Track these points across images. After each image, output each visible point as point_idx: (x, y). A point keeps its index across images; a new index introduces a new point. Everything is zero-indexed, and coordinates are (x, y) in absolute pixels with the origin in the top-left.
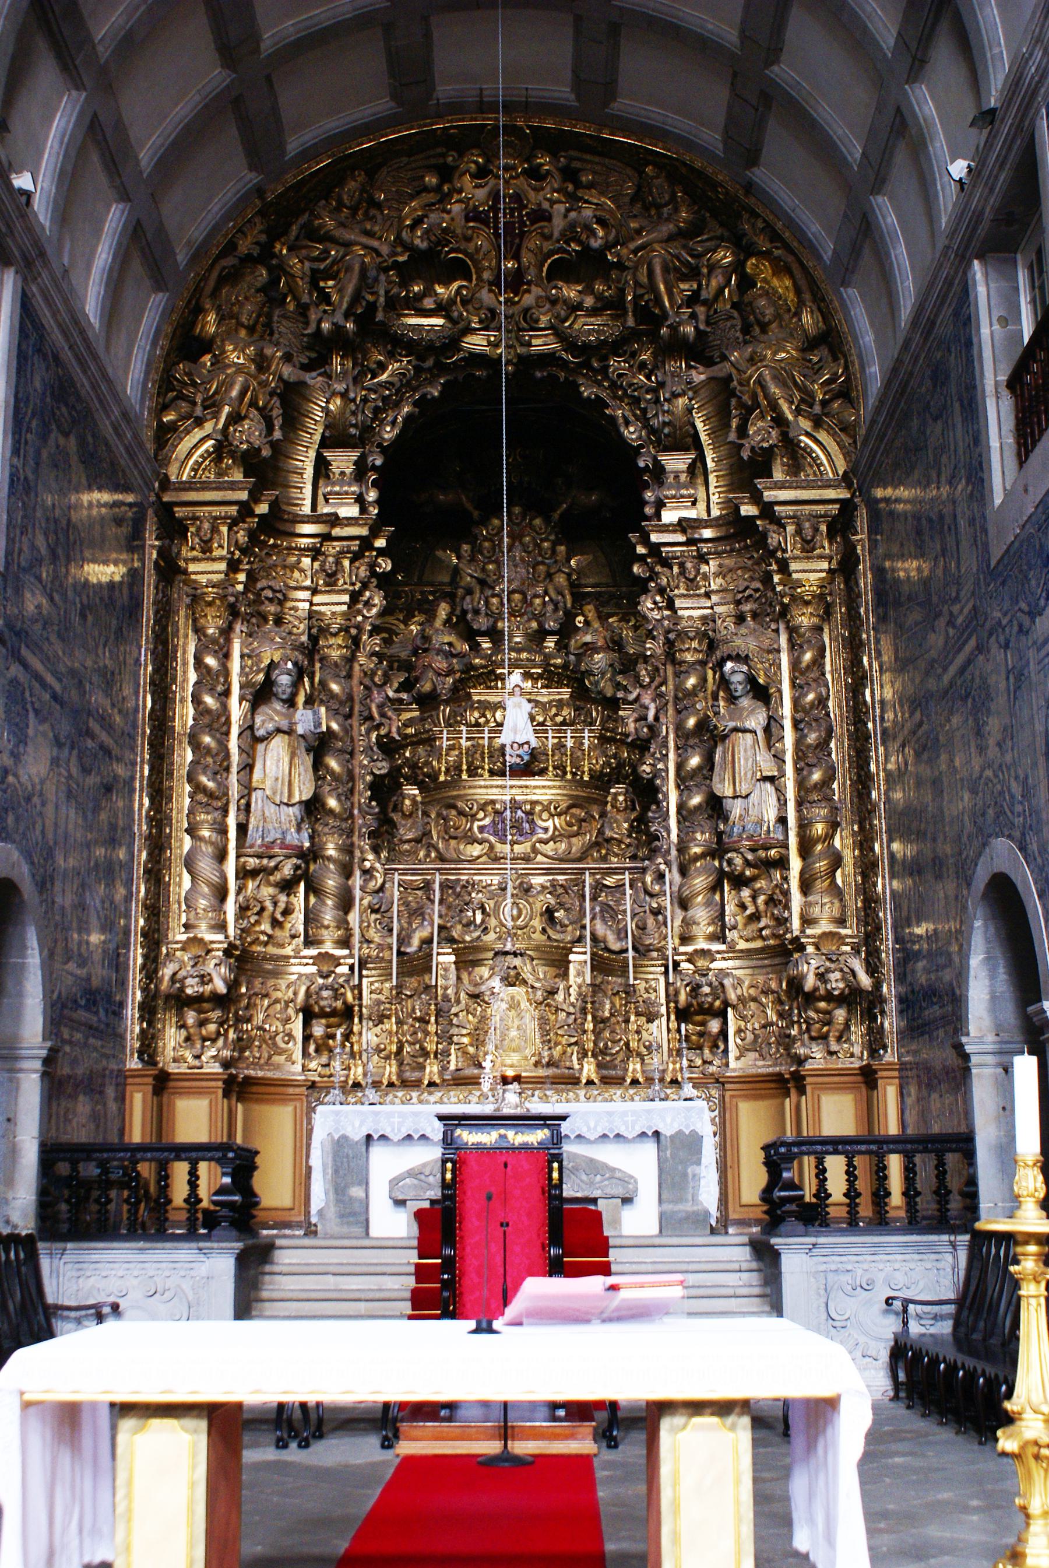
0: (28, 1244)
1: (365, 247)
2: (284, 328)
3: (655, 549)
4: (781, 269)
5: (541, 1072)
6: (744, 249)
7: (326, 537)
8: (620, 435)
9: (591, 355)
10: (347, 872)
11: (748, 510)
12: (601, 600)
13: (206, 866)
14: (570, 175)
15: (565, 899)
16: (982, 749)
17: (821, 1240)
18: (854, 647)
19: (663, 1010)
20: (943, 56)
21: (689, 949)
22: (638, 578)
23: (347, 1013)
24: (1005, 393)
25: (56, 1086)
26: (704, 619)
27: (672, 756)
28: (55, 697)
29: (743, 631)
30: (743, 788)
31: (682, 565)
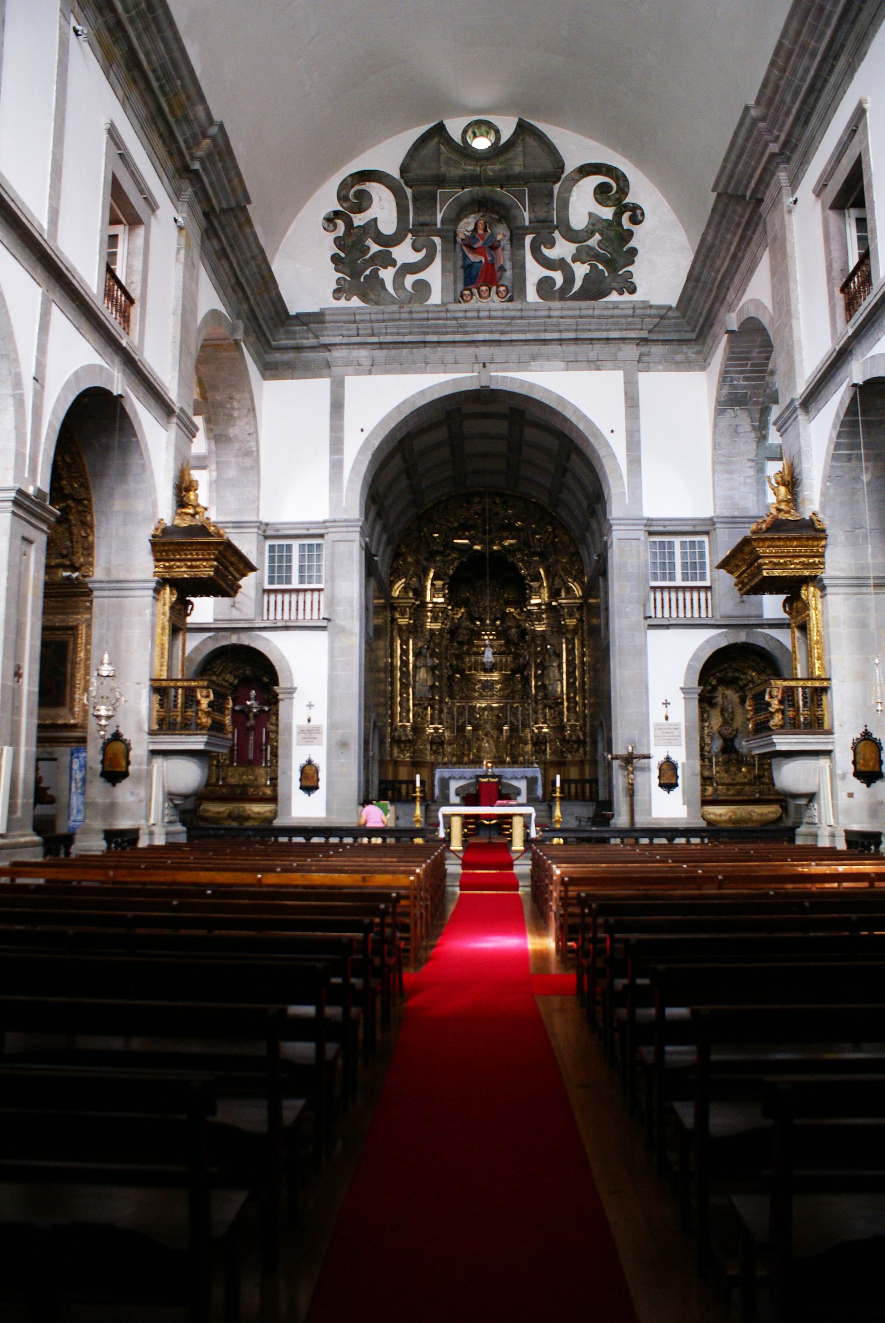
30: (552, 682)
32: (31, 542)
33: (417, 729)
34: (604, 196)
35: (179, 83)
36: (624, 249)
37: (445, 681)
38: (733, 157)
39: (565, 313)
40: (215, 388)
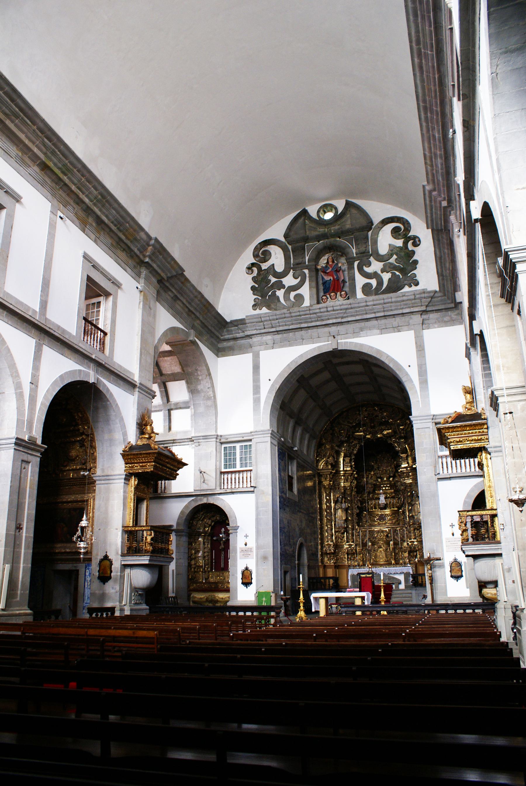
30: (417, 514)
32: (28, 462)
33: (338, 546)
34: (397, 234)
35: (127, 225)
36: (411, 262)
37: (355, 516)
38: (429, 211)
39: (375, 302)
40: (187, 365)
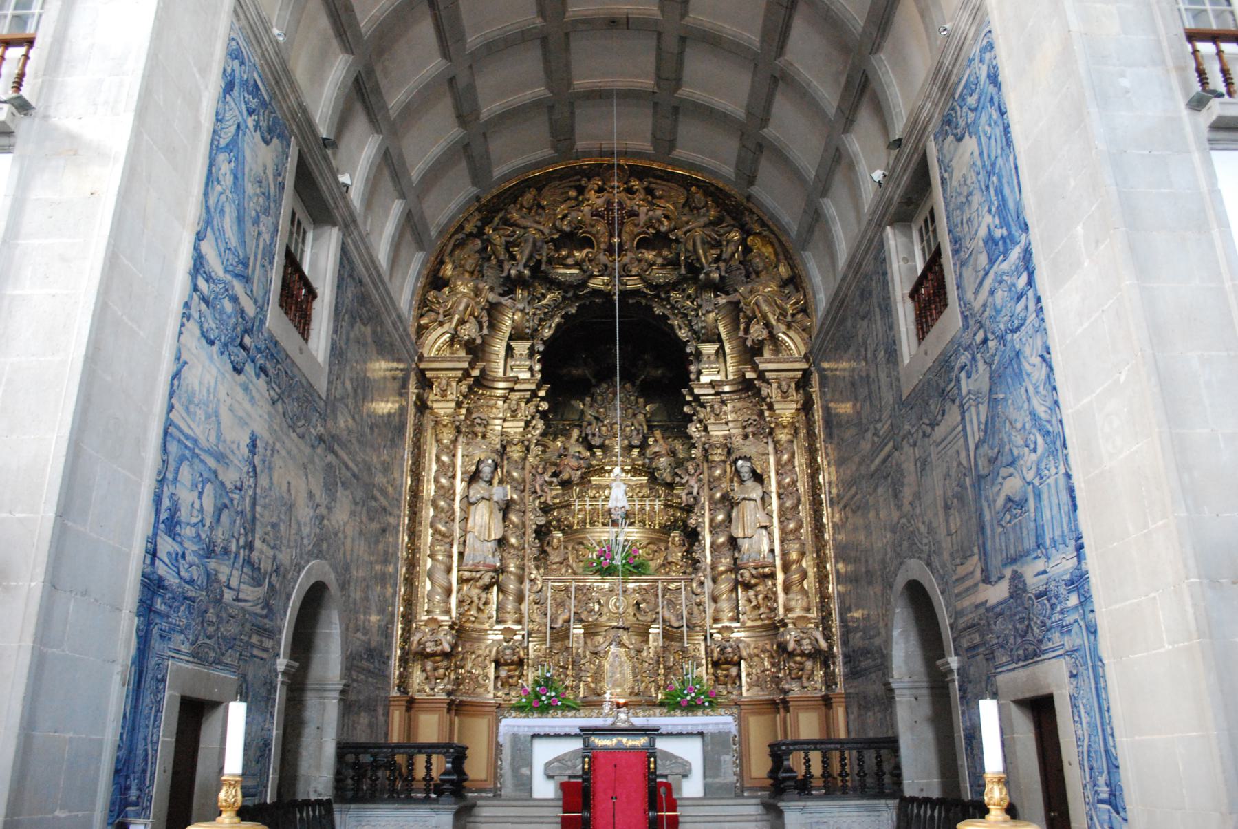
0: (326, 805)
1: (535, 229)
2: (489, 273)
3: (697, 398)
4: (767, 241)
5: (633, 699)
6: (746, 232)
7: (512, 390)
8: (676, 335)
9: (660, 290)
10: (521, 580)
11: (750, 375)
12: (665, 430)
13: (440, 576)
14: (649, 191)
15: (646, 596)
16: (899, 507)
17: (809, 803)
18: (812, 452)
19: (704, 661)
20: (865, 119)
21: (719, 626)
22: (686, 415)
23: (520, 663)
24: (909, 301)
25: (348, 706)
26: (725, 437)
27: (707, 514)
28: (354, 475)
29: (747, 442)
30: (749, 532)
31: (712, 407)
